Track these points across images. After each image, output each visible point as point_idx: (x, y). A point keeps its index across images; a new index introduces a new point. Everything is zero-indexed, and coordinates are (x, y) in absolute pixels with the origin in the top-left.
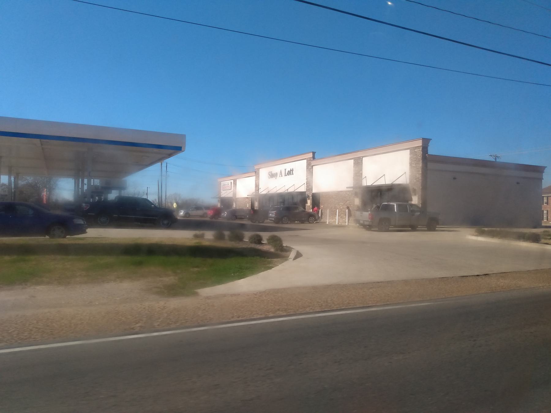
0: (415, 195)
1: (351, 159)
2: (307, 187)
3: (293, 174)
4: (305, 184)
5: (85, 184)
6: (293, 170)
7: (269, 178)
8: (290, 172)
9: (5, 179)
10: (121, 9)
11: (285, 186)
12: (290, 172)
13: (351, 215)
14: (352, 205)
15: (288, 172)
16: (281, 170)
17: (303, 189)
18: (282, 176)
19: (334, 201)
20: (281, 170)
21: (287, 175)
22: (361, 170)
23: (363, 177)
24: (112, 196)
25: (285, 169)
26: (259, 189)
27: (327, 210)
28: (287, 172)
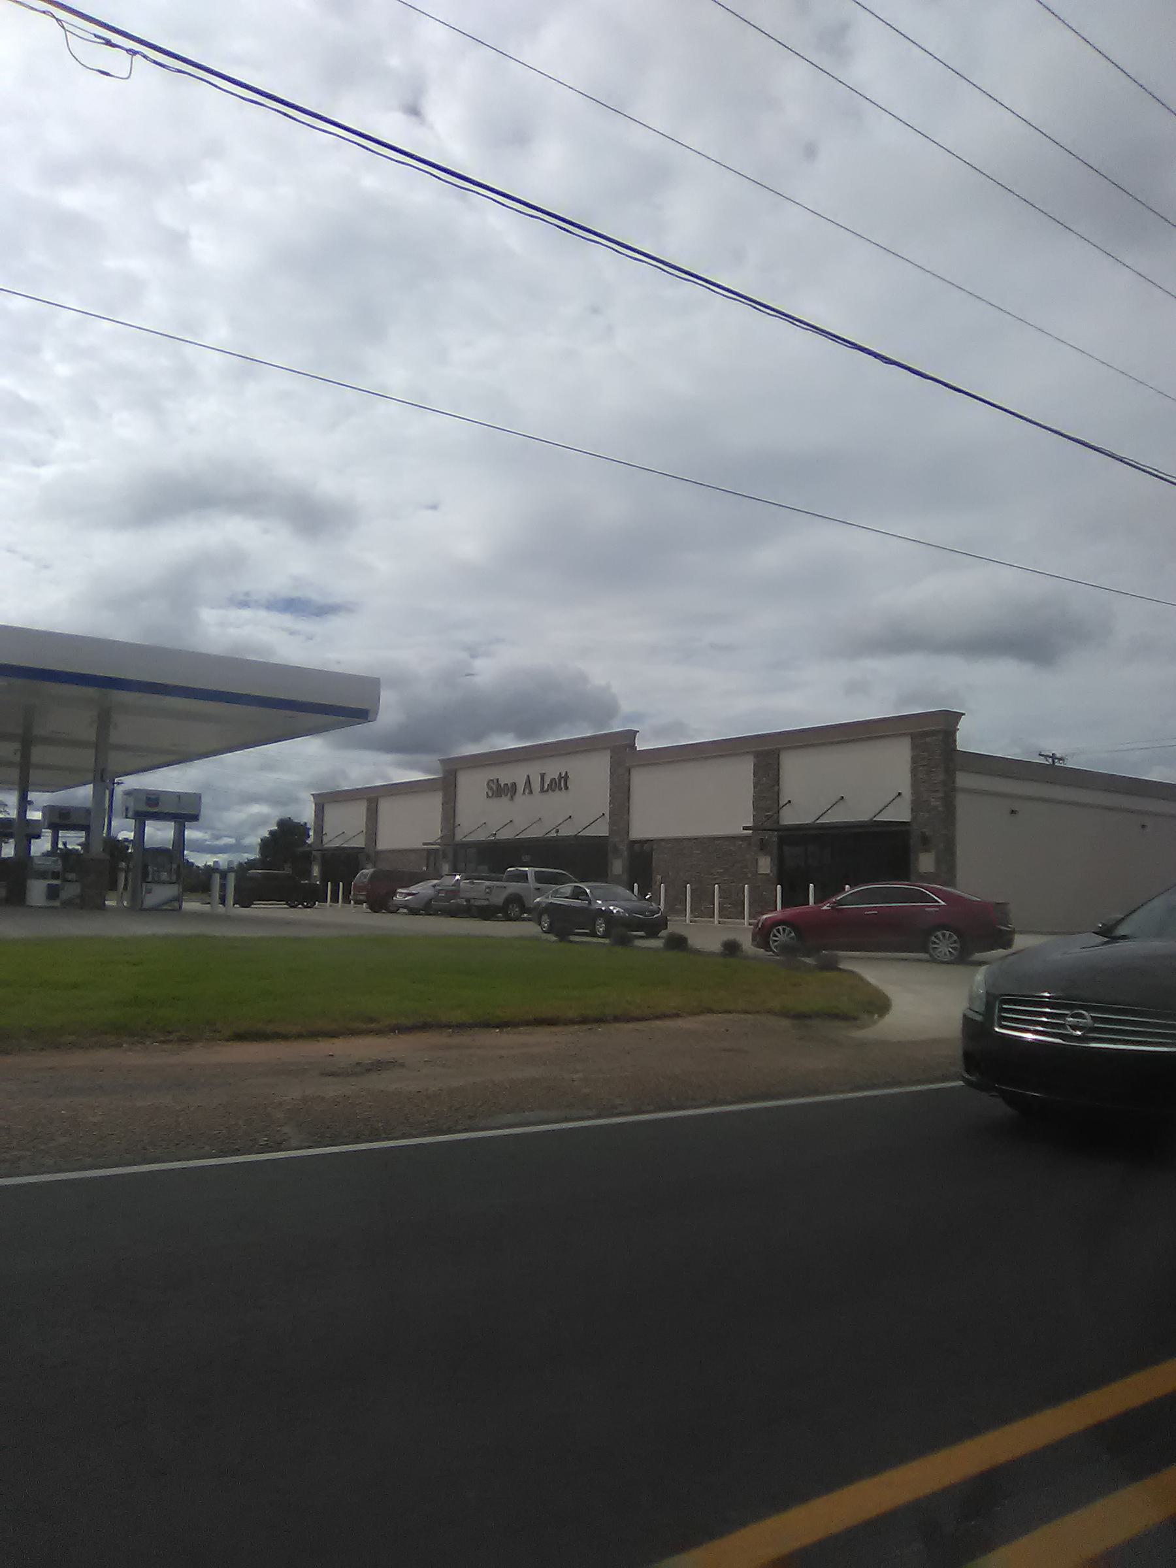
0: (927, 851)
1: (605, 749)
2: (612, 823)
3: (567, 788)
4: (607, 815)
5: (578, 894)
6: (566, 777)
7: (488, 796)
8: (561, 783)
9: (2, 830)
10: (812, 64)
11: (570, 817)
12: (561, 783)
13: (535, 874)
14: (750, 875)
15: (551, 782)
16: (528, 776)
17: (602, 829)
18: (531, 792)
19: (695, 863)
20: (528, 776)
21: (547, 791)
22: (777, 781)
23: (782, 802)
24: (727, 952)
25: (543, 776)
26: (454, 828)
27: (1001, 930)
28: (547, 782)
